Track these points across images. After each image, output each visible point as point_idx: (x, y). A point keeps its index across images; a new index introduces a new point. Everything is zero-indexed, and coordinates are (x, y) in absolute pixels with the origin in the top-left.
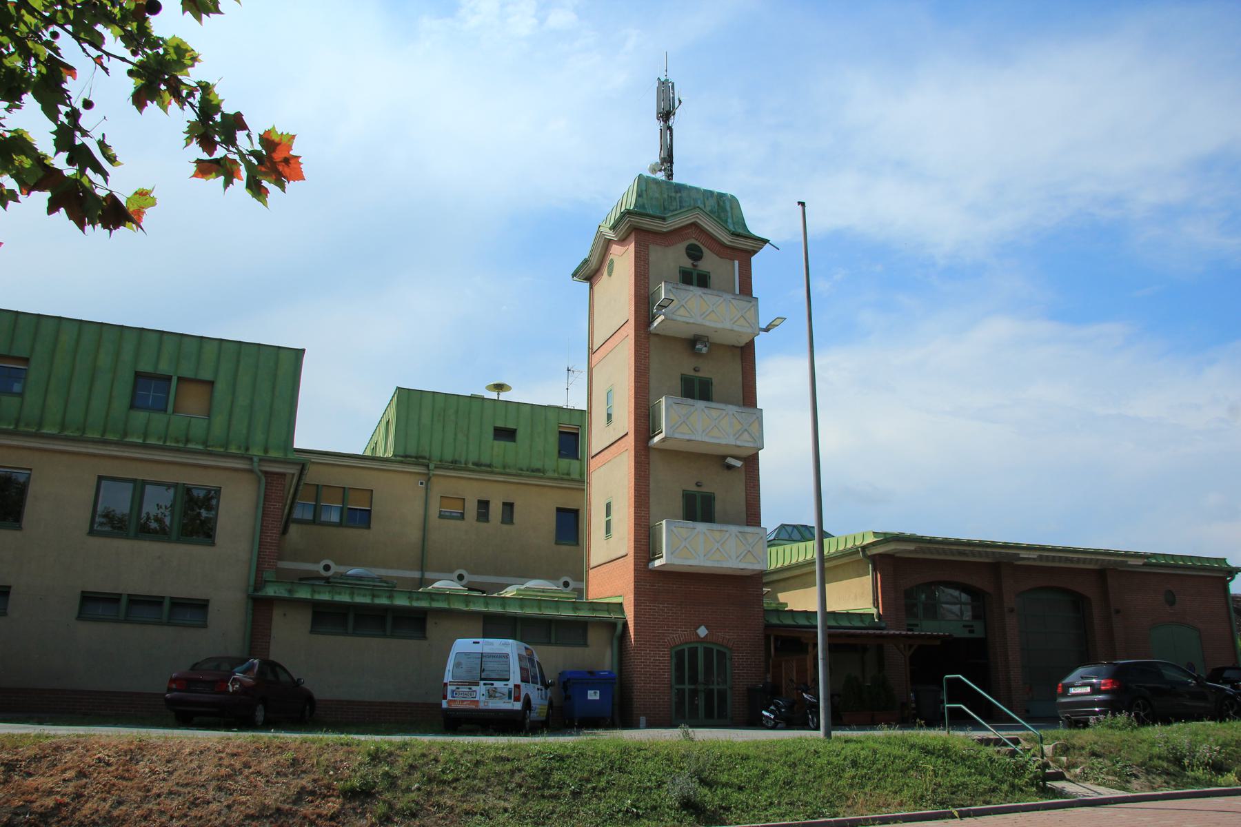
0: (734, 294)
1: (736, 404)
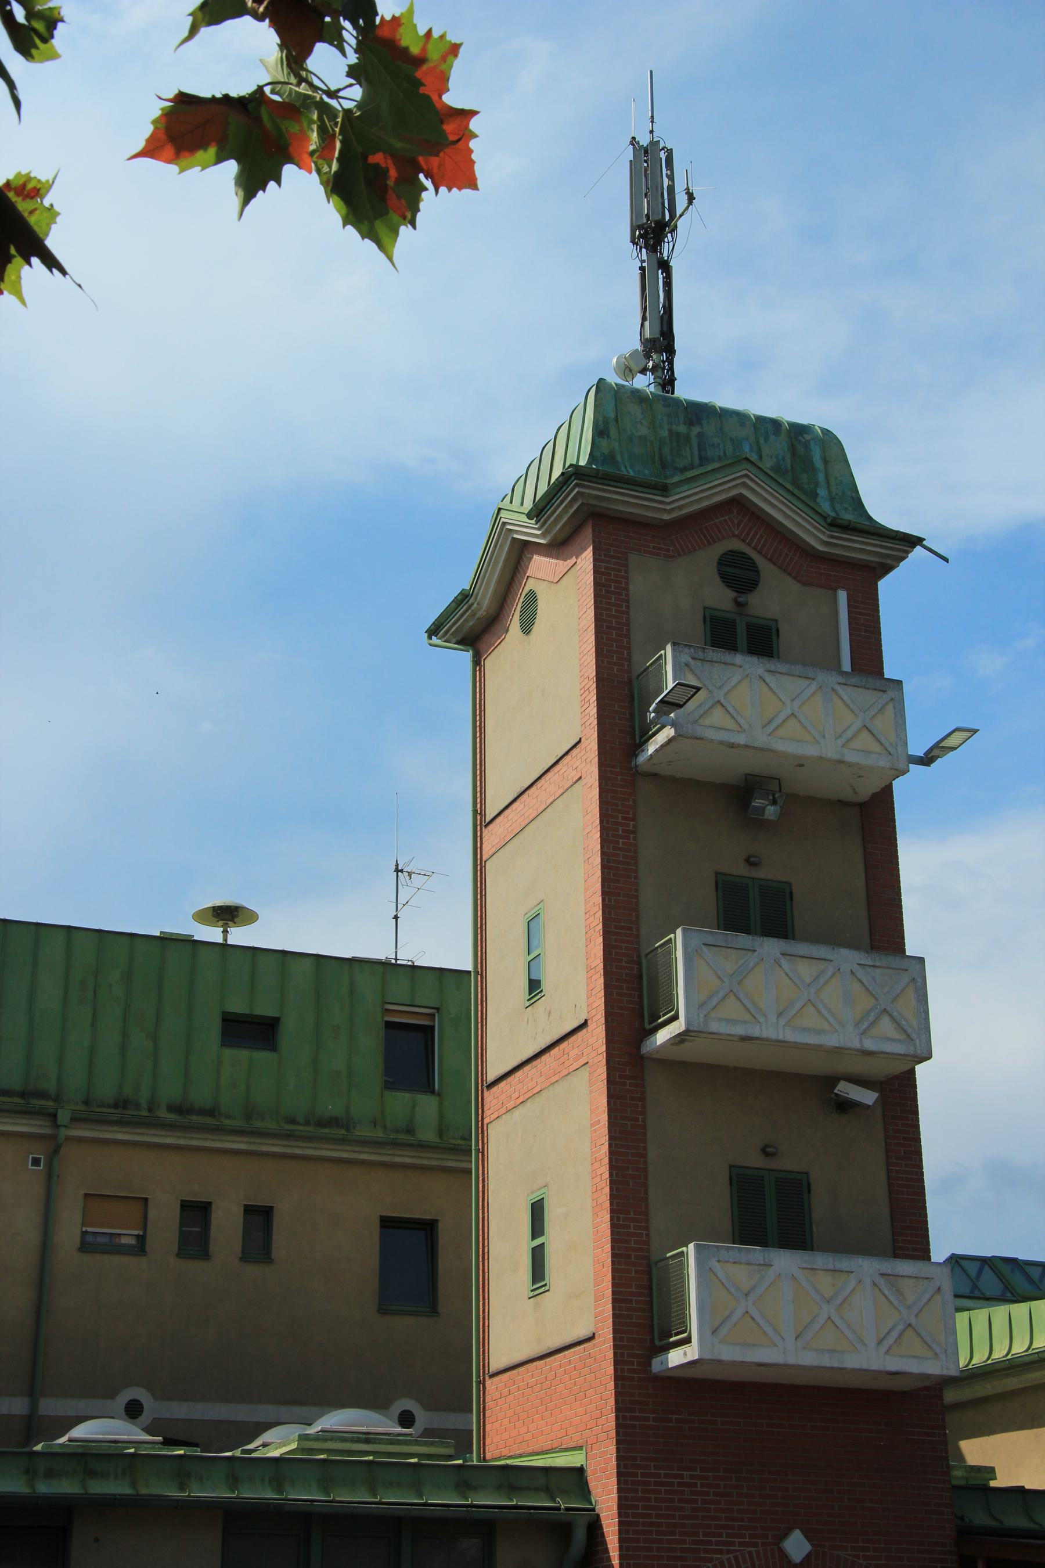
0: (837, 667)
1: (855, 946)
